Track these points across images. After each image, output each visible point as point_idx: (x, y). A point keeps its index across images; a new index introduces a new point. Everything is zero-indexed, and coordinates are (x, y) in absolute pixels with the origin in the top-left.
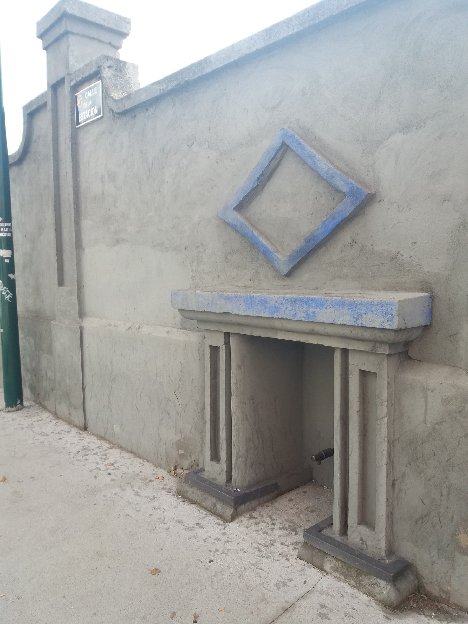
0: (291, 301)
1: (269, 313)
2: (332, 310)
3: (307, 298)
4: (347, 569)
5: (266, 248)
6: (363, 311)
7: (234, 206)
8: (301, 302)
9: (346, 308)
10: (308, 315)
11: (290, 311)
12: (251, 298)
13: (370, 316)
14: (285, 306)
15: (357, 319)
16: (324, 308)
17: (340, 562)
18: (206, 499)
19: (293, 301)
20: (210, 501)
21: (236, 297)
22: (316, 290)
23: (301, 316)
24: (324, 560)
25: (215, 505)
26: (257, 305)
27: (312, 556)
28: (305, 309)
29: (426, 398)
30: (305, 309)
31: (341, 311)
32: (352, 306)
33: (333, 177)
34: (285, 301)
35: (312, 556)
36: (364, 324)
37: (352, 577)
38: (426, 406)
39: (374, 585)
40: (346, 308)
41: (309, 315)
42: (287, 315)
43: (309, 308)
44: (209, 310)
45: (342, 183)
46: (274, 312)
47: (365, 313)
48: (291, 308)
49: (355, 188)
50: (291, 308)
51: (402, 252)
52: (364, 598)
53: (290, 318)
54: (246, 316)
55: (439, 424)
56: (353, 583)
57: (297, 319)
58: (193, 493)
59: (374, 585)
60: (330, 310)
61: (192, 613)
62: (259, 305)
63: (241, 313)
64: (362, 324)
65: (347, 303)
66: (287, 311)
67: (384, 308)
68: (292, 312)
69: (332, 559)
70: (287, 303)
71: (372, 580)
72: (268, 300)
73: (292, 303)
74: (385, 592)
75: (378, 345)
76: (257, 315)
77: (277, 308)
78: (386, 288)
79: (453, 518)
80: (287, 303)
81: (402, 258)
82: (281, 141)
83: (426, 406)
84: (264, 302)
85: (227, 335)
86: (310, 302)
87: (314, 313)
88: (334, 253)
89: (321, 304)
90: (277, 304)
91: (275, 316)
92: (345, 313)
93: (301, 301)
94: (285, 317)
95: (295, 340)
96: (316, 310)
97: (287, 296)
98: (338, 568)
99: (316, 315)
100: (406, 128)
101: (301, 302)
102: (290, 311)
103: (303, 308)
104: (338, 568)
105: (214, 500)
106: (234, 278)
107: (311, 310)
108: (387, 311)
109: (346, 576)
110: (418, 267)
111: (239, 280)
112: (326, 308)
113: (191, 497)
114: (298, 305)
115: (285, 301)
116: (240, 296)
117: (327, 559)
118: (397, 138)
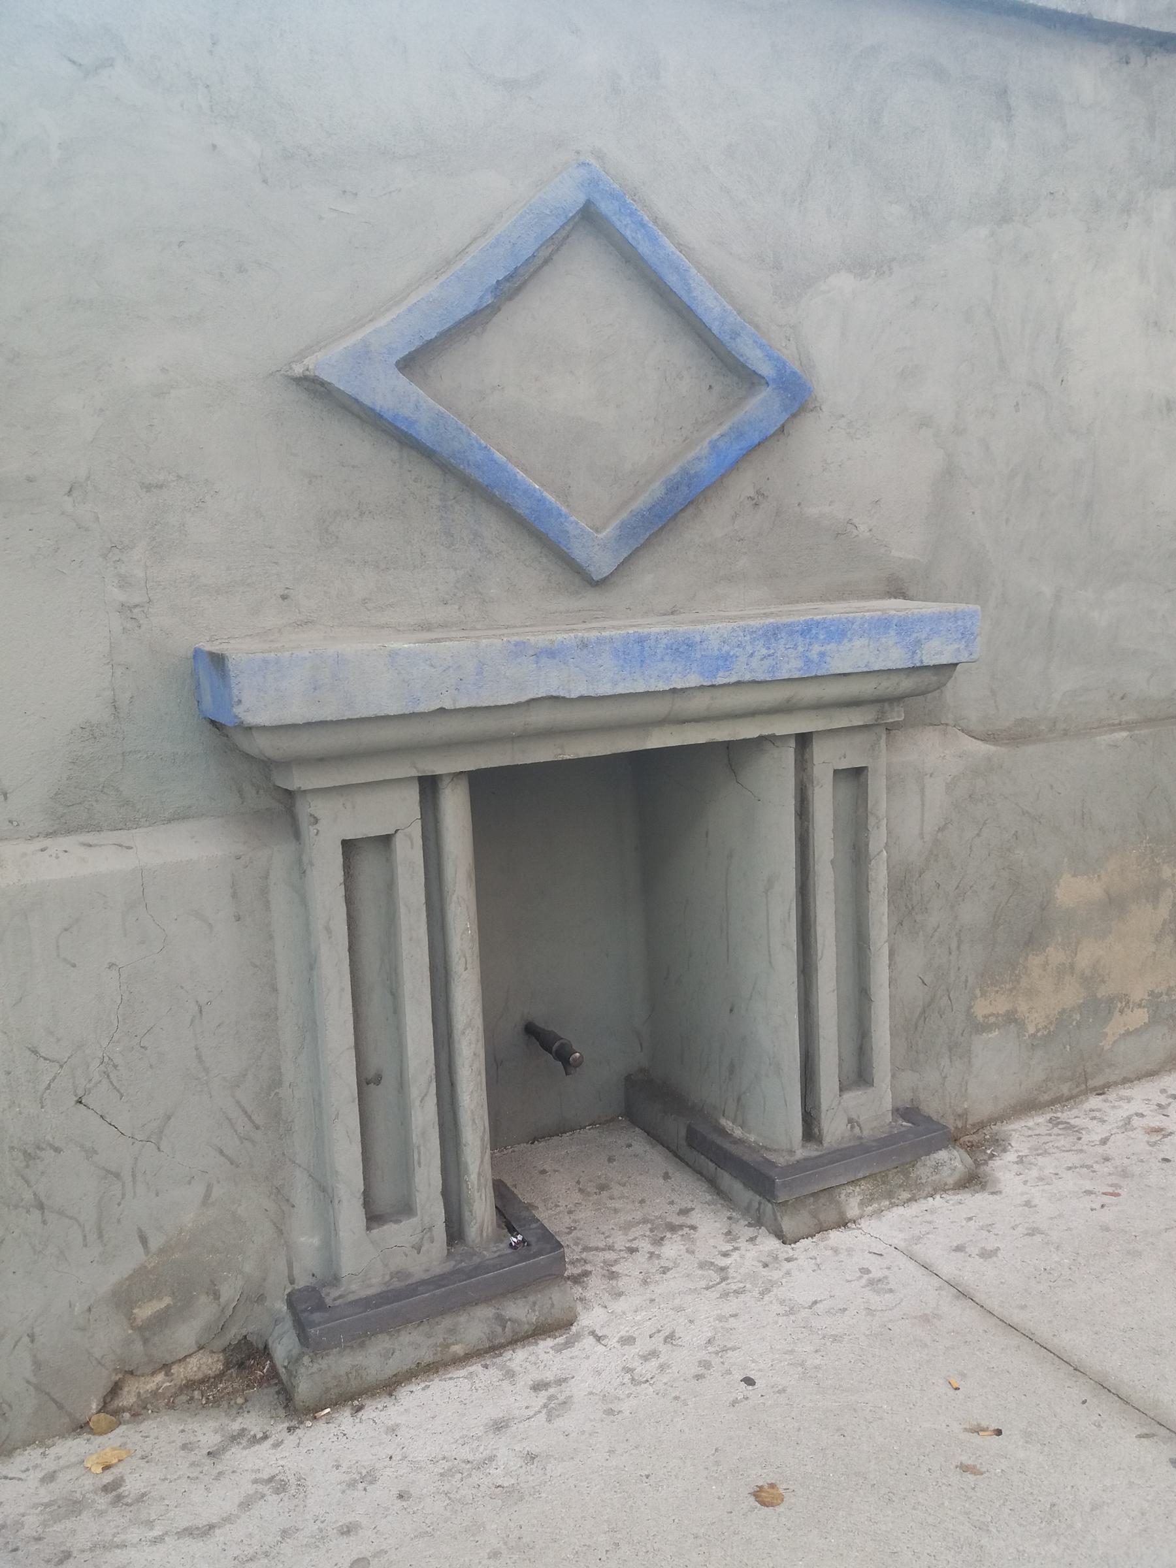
0: (765, 635)
1: (702, 674)
2: (864, 641)
3: (806, 622)
4: (884, 1183)
5: (541, 500)
6: (924, 635)
7: (399, 355)
8: (791, 633)
9: (892, 633)
10: (808, 661)
11: (762, 659)
12: (641, 640)
13: (935, 643)
14: (749, 649)
15: (914, 653)
16: (846, 640)
17: (863, 1182)
18: (452, 1331)
19: (772, 634)
20: (475, 1325)
21: (584, 645)
22: (672, 613)
23: (791, 667)
24: (838, 1203)
25: (501, 1320)
26: (662, 660)
27: (814, 1217)
28: (801, 649)
29: (922, 791)
30: (801, 649)
31: (883, 640)
32: (903, 627)
33: (735, 335)
34: (748, 638)
35: (814, 1215)
36: (927, 661)
37: (901, 1186)
38: (923, 805)
39: (937, 1168)
40: (892, 633)
41: (812, 662)
42: (752, 671)
43: (810, 644)
44: (463, 703)
45: (759, 354)
46: (718, 670)
47: (928, 639)
48: (764, 651)
49: (788, 371)
50: (764, 651)
51: (855, 521)
52: (937, 1201)
53: (761, 677)
54: (621, 695)
55: (940, 830)
56: (906, 1195)
57: (780, 676)
58: (389, 1354)
59: (936, 1167)
60: (858, 643)
61: (964, 1436)
62: (667, 658)
63: (605, 689)
64: (921, 661)
65: (895, 621)
66: (754, 663)
67: (959, 623)
68: (770, 661)
69: (850, 1189)
70: (752, 641)
71: (928, 1163)
72: (698, 639)
73: (769, 639)
74: (957, 1163)
75: (886, 705)
76: (662, 686)
77: (726, 658)
78: (824, 597)
79: (967, 981)
80: (752, 641)
81: (855, 532)
82: (582, 199)
83: (923, 805)
84: (683, 649)
85: (429, 786)
86: (814, 631)
87: (822, 655)
88: (716, 523)
89: (839, 632)
90: (726, 648)
91: (720, 681)
92: (890, 643)
93: (791, 630)
94: (748, 677)
95: (702, 740)
96: (829, 647)
97: (755, 623)
98: (871, 1194)
99: (828, 659)
100: (861, 267)
101: (791, 633)
102: (762, 659)
103: (795, 647)
104: (871, 1194)
105: (485, 1312)
106: (364, 601)
107: (816, 648)
108: (965, 628)
109: (890, 1195)
110: (883, 550)
111: (391, 605)
112: (850, 640)
113: (394, 1366)
114: (782, 642)
115: (748, 638)
116: (600, 642)
117: (843, 1196)
118: (843, 282)
